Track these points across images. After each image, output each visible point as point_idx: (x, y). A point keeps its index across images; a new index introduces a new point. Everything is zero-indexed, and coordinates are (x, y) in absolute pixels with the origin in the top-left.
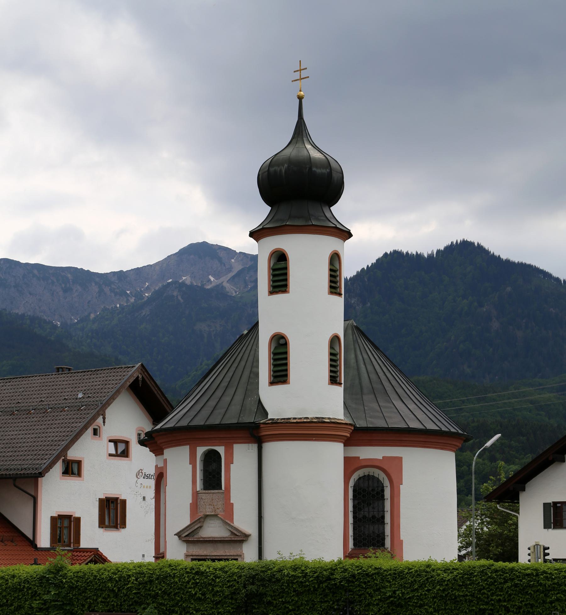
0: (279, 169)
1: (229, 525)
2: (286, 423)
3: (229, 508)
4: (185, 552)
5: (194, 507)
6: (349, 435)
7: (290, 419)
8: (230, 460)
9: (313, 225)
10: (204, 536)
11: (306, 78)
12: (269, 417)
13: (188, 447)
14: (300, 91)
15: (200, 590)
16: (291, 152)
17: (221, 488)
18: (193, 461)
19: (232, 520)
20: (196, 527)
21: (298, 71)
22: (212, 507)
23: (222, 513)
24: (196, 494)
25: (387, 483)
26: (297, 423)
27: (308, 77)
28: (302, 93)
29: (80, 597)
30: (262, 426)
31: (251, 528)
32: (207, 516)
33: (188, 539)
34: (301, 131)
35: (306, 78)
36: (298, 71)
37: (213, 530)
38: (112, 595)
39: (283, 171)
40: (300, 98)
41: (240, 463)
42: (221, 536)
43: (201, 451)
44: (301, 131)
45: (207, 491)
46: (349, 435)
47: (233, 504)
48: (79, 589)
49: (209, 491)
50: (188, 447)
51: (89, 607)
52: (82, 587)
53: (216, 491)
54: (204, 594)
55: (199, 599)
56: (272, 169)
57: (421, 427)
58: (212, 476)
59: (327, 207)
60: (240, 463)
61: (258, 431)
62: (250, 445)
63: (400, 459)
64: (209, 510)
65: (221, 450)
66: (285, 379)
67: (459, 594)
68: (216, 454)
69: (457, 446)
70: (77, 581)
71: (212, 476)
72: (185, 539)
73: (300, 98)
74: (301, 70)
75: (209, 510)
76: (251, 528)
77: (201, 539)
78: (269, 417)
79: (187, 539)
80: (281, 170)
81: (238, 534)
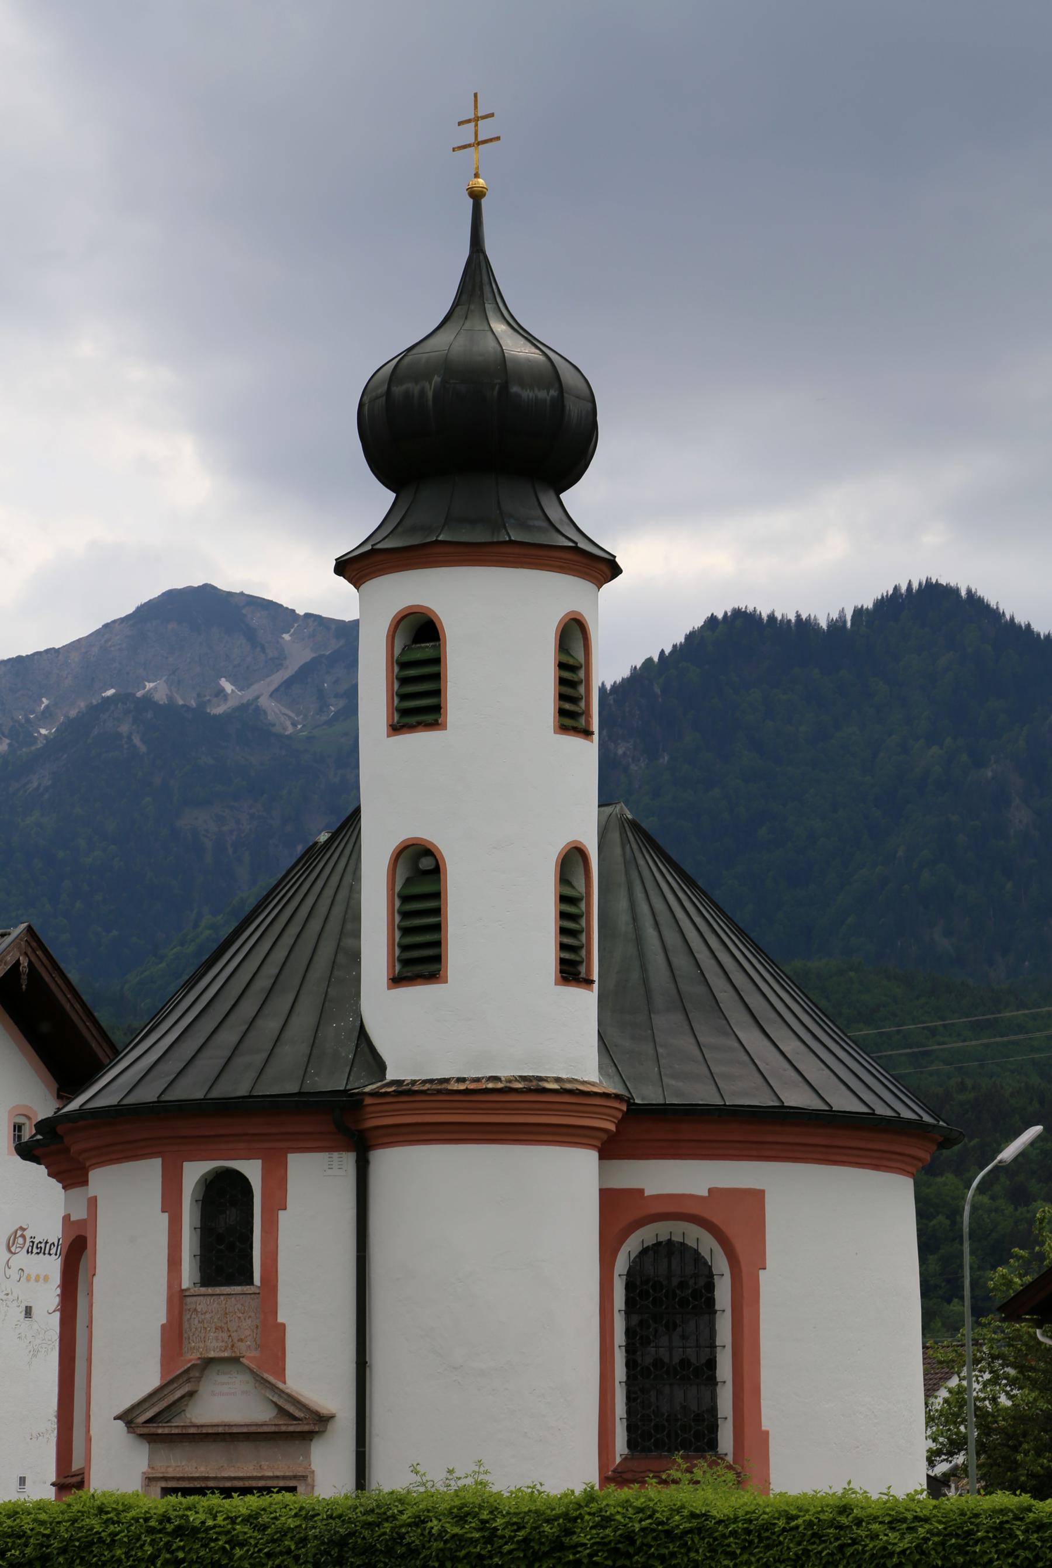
1: (273, 1387)
2: (438, 1092)
3: (273, 1339)
5: (174, 1336)
7: (447, 1081)
8: (277, 1201)
9: (437, 542)
12: (390, 1076)
14: (476, 176)
17: (250, 1281)
18: (171, 1202)
19: (281, 1374)
20: (178, 1394)
21: (469, 121)
22: (225, 1335)
25: (721, 1265)
26: (467, 1092)
30: (368, 1101)
32: (208, 1363)
33: (153, 1430)
34: (477, 285)
36: (469, 121)
37: (226, 1402)
39: (430, 394)
40: (476, 196)
42: (248, 1421)
43: (194, 1173)
44: (477, 285)
45: (210, 1290)
47: (283, 1325)
49: (218, 1290)
53: (238, 1289)
56: (398, 390)
58: (226, 1245)
62: (335, 1155)
64: (215, 1344)
65: (252, 1170)
66: (433, 967)
68: (241, 1182)
71: (226, 1245)
72: (145, 1431)
73: (476, 196)
74: (477, 119)
75: (215, 1344)
78: (390, 1076)
79: (152, 1429)
80: (423, 393)
81: (298, 1414)
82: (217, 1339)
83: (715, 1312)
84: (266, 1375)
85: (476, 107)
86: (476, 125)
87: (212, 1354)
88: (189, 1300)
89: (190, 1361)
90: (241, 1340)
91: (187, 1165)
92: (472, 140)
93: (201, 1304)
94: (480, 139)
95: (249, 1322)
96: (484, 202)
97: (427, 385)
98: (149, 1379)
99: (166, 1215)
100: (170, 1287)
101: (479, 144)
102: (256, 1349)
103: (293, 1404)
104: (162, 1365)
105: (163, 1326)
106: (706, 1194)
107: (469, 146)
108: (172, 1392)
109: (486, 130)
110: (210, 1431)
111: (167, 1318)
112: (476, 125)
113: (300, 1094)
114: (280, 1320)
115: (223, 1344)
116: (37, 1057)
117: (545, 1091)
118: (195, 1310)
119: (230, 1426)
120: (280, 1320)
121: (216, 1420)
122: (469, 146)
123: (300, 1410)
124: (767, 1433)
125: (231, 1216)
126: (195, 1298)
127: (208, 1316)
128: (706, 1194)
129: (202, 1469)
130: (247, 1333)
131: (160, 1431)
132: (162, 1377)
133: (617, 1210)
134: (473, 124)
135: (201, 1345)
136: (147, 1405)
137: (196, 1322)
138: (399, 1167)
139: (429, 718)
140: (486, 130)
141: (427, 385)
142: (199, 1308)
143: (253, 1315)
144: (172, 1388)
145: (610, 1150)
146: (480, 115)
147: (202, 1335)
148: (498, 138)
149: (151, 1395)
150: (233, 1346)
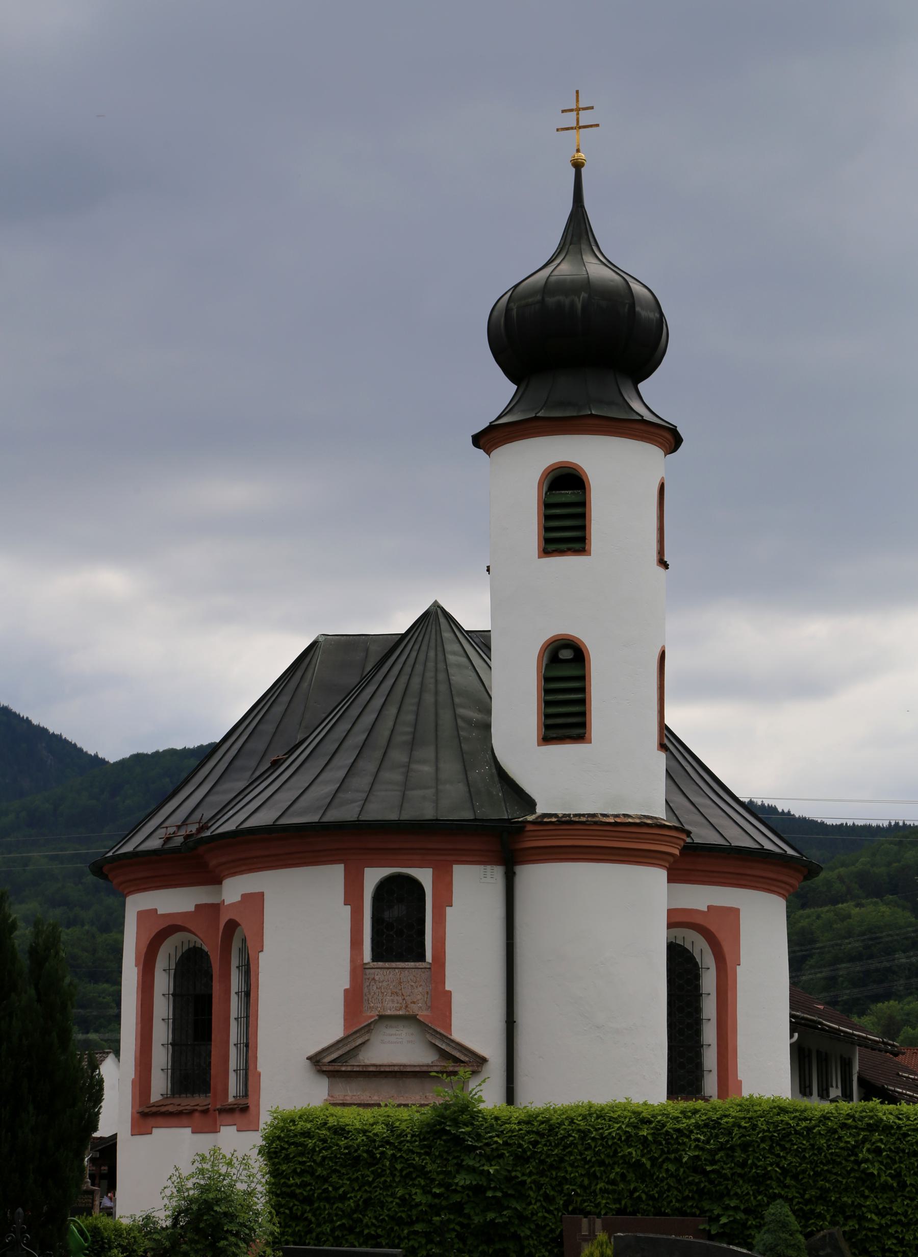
0: (567, 302)
1: (447, 1038)
2: (566, 823)
3: (441, 1001)
4: (326, 1097)
5: (354, 999)
6: (677, 852)
7: (594, 815)
8: (444, 899)
9: (592, 415)
10: (367, 1062)
11: (591, 126)
12: (540, 810)
13: (342, 866)
14: (578, 151)
15: (888, 1167)
16: (565, 269)
17: (421, 957)
18: (352, 896)
19: (449, 1027)
20: (359, 1041)
21: (571, 110)
22: (400, 999)
23: (425, 1013)
24: (358, 970)
25: (708, 961)
26: (616, 824)
27: (597, 125)
28: (582, 155)
29: (543, 1180)
30: (529, 827)
31: (489, 1046)
32: (382, 1018)
33: (337, 1068)
34: (578, 232)
35: (591, 126)
36: (571, 110)
37: (396, 1048)
38: (631, 1176)
39: (579, 306)
40: (578, 166)
41: (467, 907)
42: (412, 1063)
43: (373, 876)
44: (578, 232)
45: (380, 964)
46: (677, 852)
47: (450, 992)
48: (542, 1162)
49: (394, 965)
50: (342, 866)
51: (566, 1204)
52: (548, 1156)
53: (411, 964)
54: (897, 1176)
55: (886, 1187)
56: (551, 301)
57: (720, 841)
58: (399, 930)
59: (630, 384)
60: (467, 907)
61: (511, 835)
62: (489, 867)
63: (734, 913)
64: (390, 1005)
65: (424, 876)
66: (579, 731)
67: (440, 1216)
68: (416, 887)
69: (791, 886)
70: (535, 1144)
71: (399, 930)
72: (331, 1068)
73: (578, 166)
74: (578, 110)
75: (390, 1005)
76: (489, 1046)
77: (371, 1069)
78: (540, 810)
79: (335, 1067)
80: (572, 304)
81: (463, 1058)
82: (393, 1001)
83: (701, 995)
84: (438, 1030)
85: (577, 101)
86: (578, 114)
87: (389, 1012)
88: (368, 971)
89: (372, 1017)
90: (414, 1003)
91: (367, 870)
92: (574, 125)
93: (379, 975)
94: (581, 124)
95: (420, 989)
96: (584, 170)
97: (576, 299)
98: (330, 1029)
99: (349, 907)
100: (352, 961)
101: (580, 128)
102: (427, 1010)
103: (460, 1051)
104: (345, 1020)
105: (346, 991)
106: (706, 909)
107: (572, 128)
108: (354, 1040)
109: (586, 118)
110: (387, 1069)
111: (351, 985)
112: (578, 114)
113: (475, 820)
114: (447, 988)
115: (399, 1005)
116: (507, 770)
117: (647, 825)
118: (374, 979)
119: (405, 1066)
120: (447, 988)
121: (385, 1061)
122: (572, 128)
123: (465, 1055)
124: (741, 1081)
125: (396, 912)
126: (373, 971)
127: (385, 984)
128: (706, 909)
129: (376, 1098)
130: (419, 997)
131: (343, 1069)
132: (346, 1027)
133: (677, 920)
134: (574, 113)
135: (379, 1005)
136: (333, 1049)
137: (375, 988)
138: (538, 878)
139: (577, 546)
140: (586, 118)
141: (576, 299)
142: (377, 978)
143: (423, 984)
144: (355, 1036)
145: (678, 874)
146: (581, 106)
147: (380, 998)
148: (597, 125)
149: (338, 1042)
150: (407, 1006)
